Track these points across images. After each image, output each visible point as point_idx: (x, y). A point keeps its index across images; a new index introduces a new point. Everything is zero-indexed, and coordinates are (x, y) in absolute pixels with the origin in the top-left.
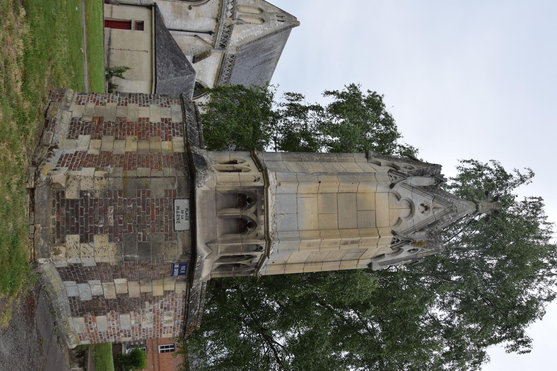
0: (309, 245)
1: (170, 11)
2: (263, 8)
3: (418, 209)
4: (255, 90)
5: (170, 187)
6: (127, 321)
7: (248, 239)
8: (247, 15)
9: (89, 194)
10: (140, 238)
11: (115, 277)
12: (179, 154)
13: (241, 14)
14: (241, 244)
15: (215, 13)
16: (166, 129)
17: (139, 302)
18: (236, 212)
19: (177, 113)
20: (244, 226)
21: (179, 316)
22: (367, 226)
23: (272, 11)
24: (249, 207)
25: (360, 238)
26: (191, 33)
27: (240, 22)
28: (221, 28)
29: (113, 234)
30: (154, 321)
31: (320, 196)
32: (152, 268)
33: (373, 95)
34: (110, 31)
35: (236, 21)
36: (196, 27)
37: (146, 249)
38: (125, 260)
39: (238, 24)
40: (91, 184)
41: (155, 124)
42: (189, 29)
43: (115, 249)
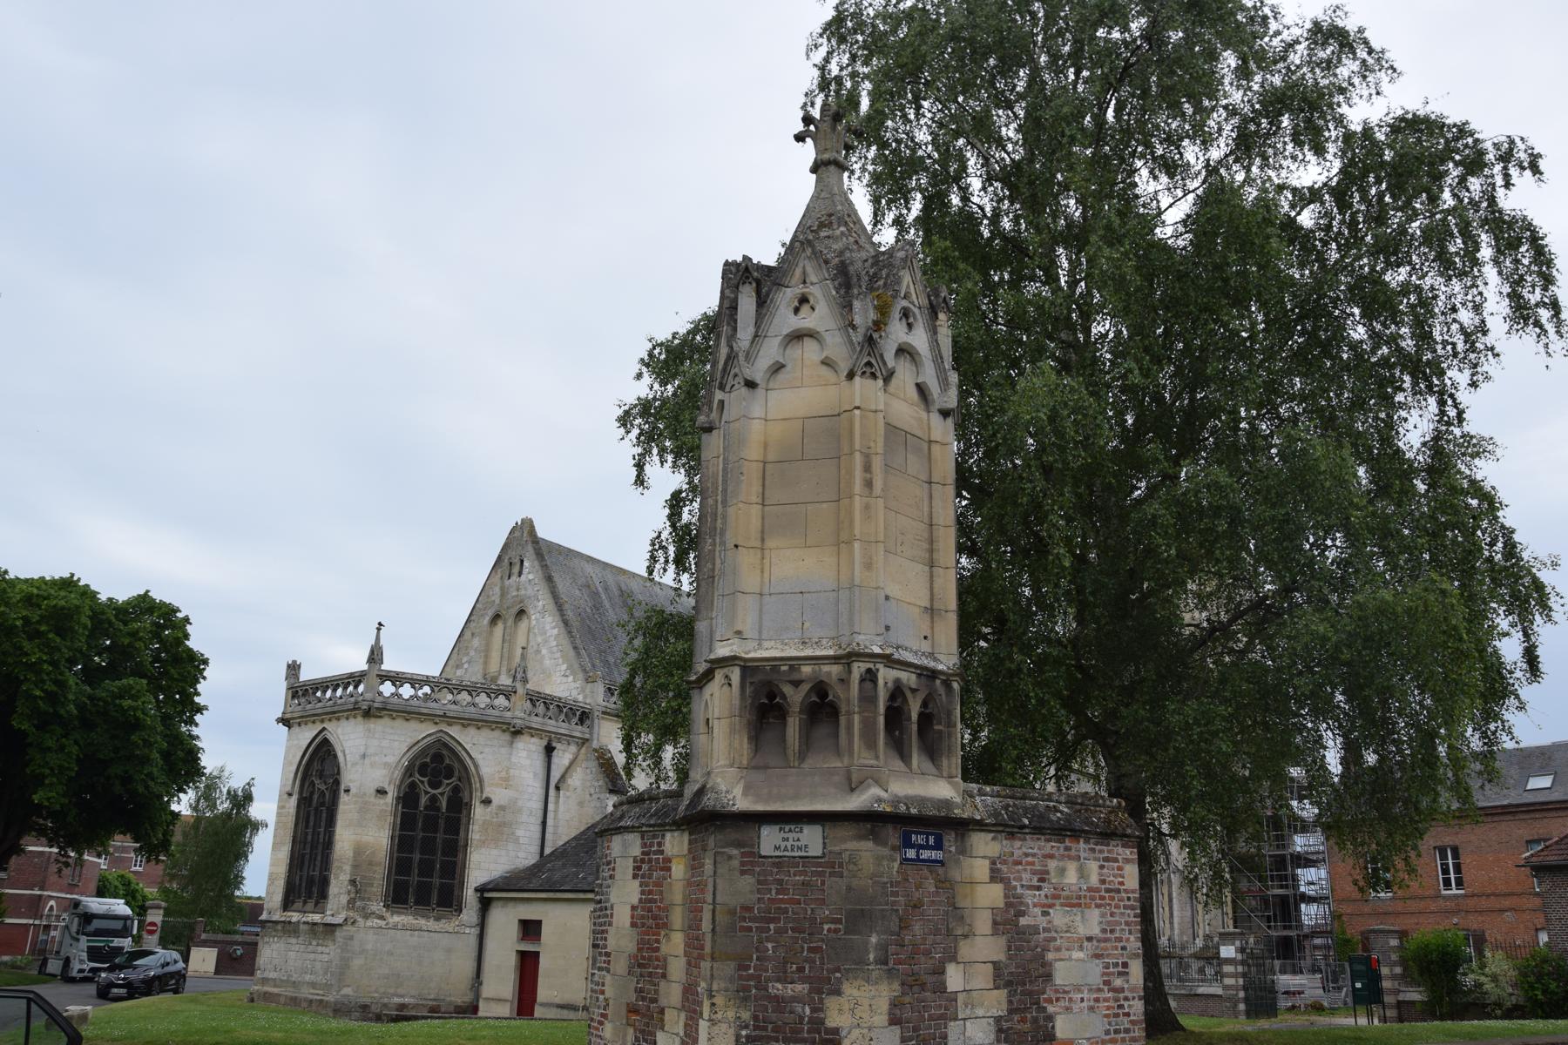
0: (868, 566)
1: (494, 852)
2: (491, 613)
3: (807, 320)
4: (634, 656)
5: (736, 863)
6: (1073, 968)
7: (848, 700)
8: (507, 655)
9: (744, 1033)
10: (836, 931)
11: (941, 988)
12: (690, 843)
13: (504, 669)
14: (856, 718)
15: (498, 737)
16: (650, 867)
17: (1020, 940)
18: (793, 726)
19: (625, 846)
20: (823, 708)
21: (1067, 849)
22: (829, 436)
23: (497, 590)
24: (784, 697)
25: (857, 455)
26: (551, 799)
27: (520, 674)
28: (536, 722)
29: (824, 986)
30: (1079, 905)
31: (769, 543)
32: (915, 906)
33: (647, 365)
34: (542, 1005)
35: (519, 685)
36: (534, 786)
37: (858, 918)
38: (886, 964)
39: (525, 680)
40: (724, 1026)
41: (643, 893)
42: (540, 805)
43: (856, 983)
